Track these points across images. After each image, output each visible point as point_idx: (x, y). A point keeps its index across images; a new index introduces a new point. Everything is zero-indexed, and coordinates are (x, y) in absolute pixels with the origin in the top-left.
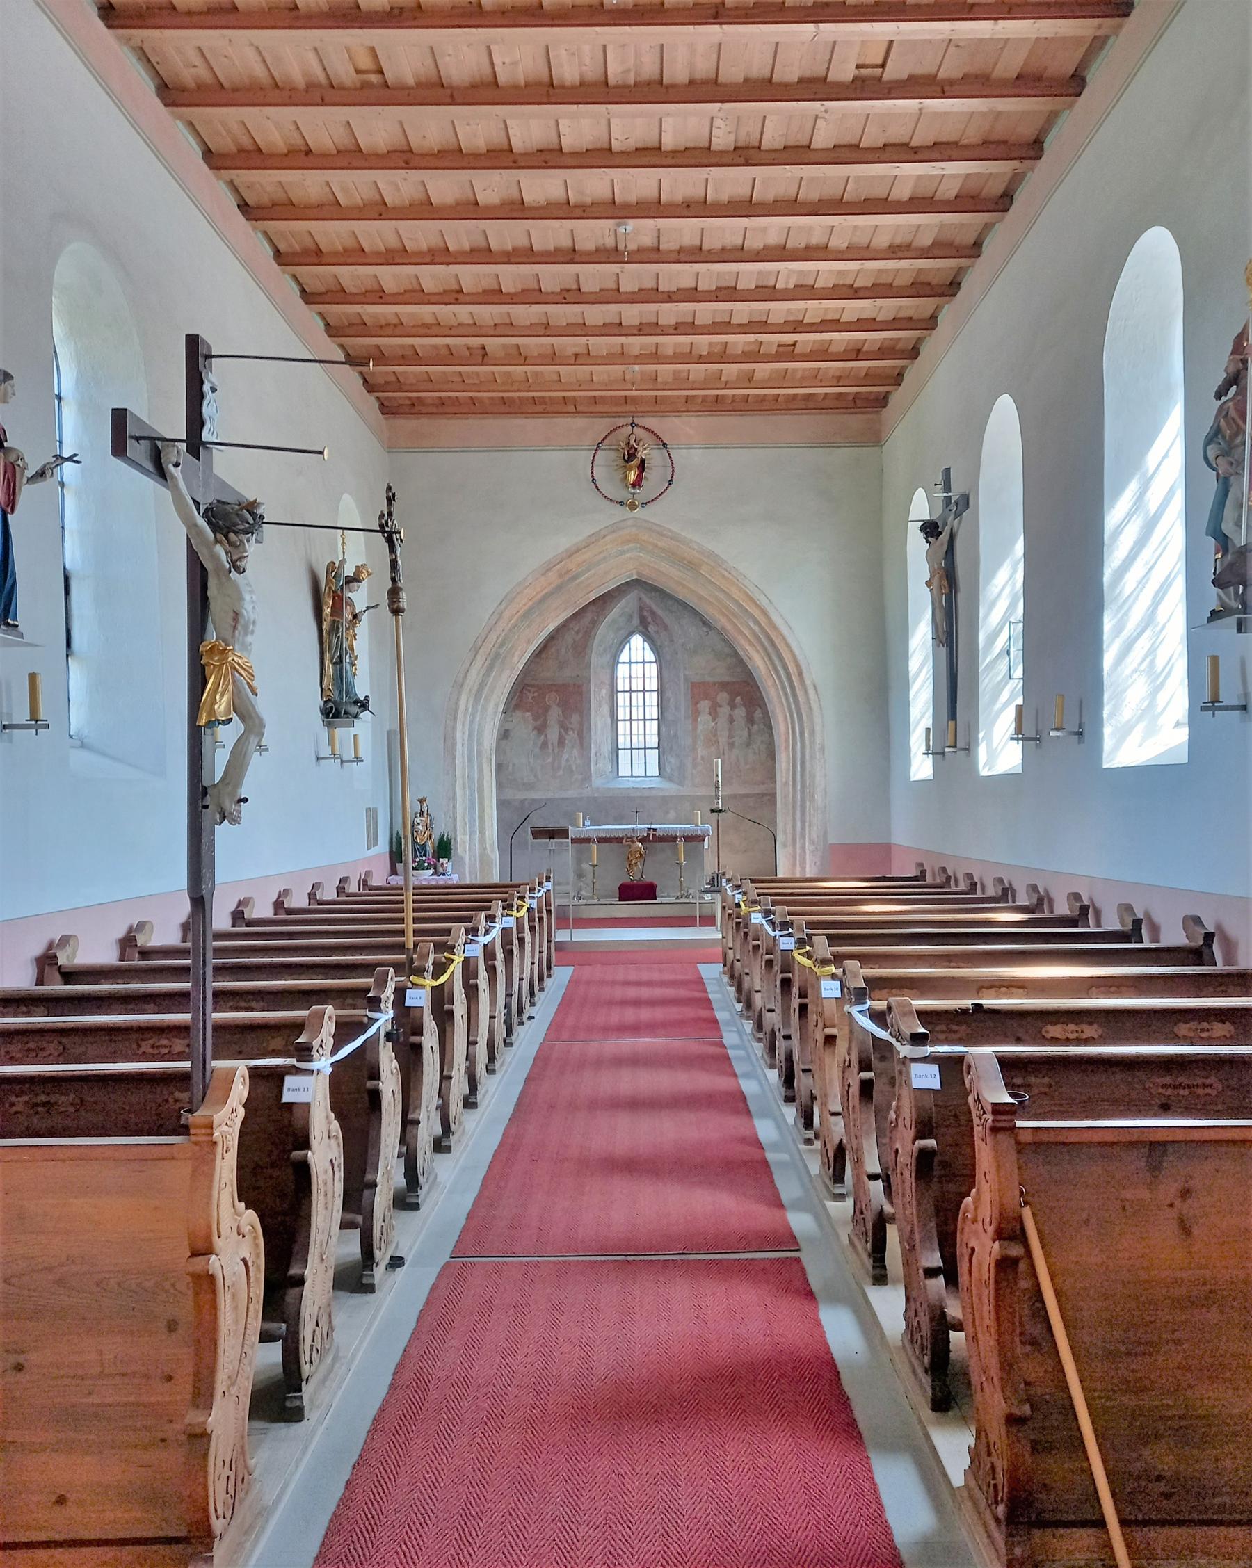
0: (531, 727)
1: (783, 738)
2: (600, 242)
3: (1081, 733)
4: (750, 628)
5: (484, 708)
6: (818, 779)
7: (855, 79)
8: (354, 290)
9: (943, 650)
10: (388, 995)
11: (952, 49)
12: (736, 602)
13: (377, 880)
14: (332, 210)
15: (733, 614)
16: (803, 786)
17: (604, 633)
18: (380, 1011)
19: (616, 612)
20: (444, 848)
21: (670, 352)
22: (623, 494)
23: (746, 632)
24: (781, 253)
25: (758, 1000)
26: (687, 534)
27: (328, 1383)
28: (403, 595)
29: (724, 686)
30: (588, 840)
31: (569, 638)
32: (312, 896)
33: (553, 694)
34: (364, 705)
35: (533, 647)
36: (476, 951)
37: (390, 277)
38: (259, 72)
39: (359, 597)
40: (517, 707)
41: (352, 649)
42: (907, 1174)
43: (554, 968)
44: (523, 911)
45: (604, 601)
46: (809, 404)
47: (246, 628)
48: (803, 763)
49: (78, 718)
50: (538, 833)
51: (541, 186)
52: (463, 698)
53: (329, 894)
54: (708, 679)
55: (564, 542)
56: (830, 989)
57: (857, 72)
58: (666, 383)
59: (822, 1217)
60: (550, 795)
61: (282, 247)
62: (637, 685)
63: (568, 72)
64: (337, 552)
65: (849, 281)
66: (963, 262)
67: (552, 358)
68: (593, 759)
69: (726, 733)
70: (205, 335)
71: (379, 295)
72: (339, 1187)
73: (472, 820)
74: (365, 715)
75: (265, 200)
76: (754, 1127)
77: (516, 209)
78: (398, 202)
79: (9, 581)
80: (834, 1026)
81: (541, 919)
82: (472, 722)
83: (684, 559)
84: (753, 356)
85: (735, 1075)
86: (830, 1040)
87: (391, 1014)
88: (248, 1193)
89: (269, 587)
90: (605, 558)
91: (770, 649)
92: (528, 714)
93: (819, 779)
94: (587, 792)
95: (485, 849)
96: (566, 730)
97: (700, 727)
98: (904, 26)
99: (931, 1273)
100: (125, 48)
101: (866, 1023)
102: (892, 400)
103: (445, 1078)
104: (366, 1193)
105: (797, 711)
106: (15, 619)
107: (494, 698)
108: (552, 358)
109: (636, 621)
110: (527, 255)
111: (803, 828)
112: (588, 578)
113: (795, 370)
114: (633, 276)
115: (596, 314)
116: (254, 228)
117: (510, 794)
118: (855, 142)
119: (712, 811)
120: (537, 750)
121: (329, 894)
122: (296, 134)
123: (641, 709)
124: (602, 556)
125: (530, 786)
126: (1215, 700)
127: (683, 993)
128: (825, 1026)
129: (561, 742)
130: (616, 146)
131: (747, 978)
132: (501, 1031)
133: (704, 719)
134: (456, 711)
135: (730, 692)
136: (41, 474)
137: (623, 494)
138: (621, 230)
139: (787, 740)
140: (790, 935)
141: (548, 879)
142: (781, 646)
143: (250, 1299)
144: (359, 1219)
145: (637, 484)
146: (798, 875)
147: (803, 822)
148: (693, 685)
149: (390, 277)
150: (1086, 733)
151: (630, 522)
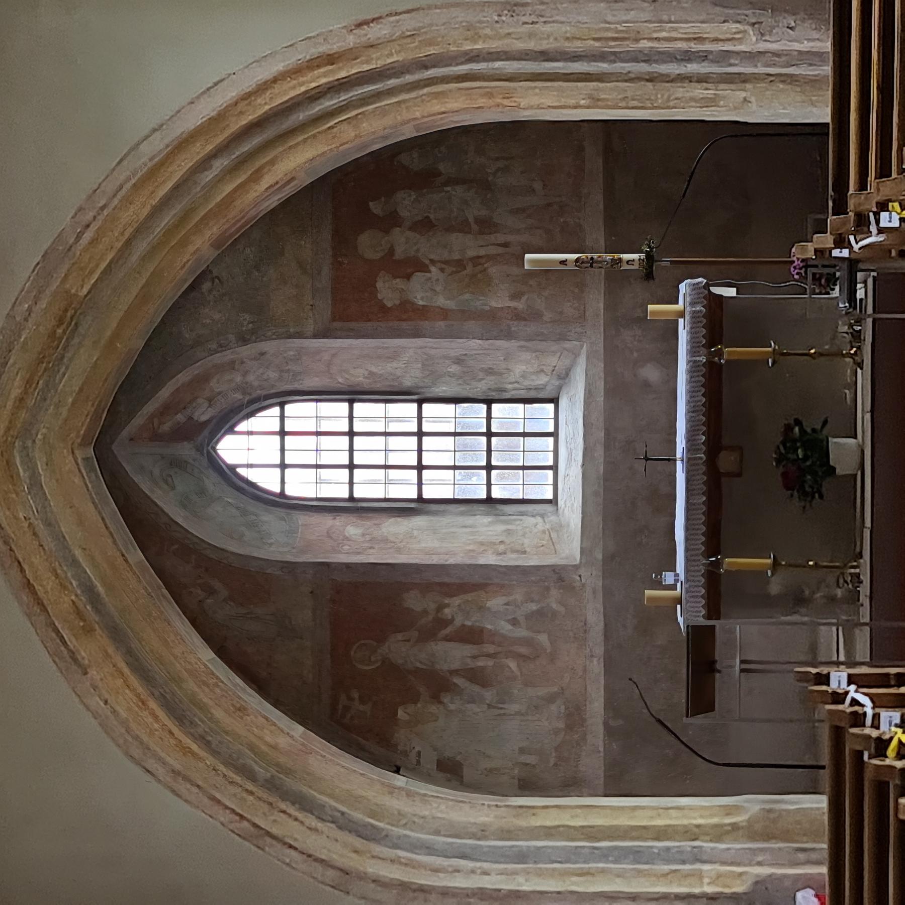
0: (433, 708)
4: (220, 179)
5: (398, 818)
17: (215, 527)
23: (229, 188)
29: (343, 242)
40: (385, 741)
45: (143, 524)
50: (701, 699)
60: (597, 667)
62: (335, 450)
68: (512, 560)
69: (456, 240)
73: (666, 856)
82: (430, 850)
83: (52, 335)
90: (48, 524)
92: (401, 713)
94: (591, 579)
95: (735, 827)
97: (441, 301)
109: (185, 450)
111: (704, 57)
112: (92, 559)
117: (592, 764)
120: (489, 695)
123: (394, 442)
124: (40, 527)
125: (575, 717)
129: (472, 636)
133: (419, 291)
134: (404, 886)
141: (824, 679)
142: (264, 105)
146: (827, 69)
147: (687, 57)
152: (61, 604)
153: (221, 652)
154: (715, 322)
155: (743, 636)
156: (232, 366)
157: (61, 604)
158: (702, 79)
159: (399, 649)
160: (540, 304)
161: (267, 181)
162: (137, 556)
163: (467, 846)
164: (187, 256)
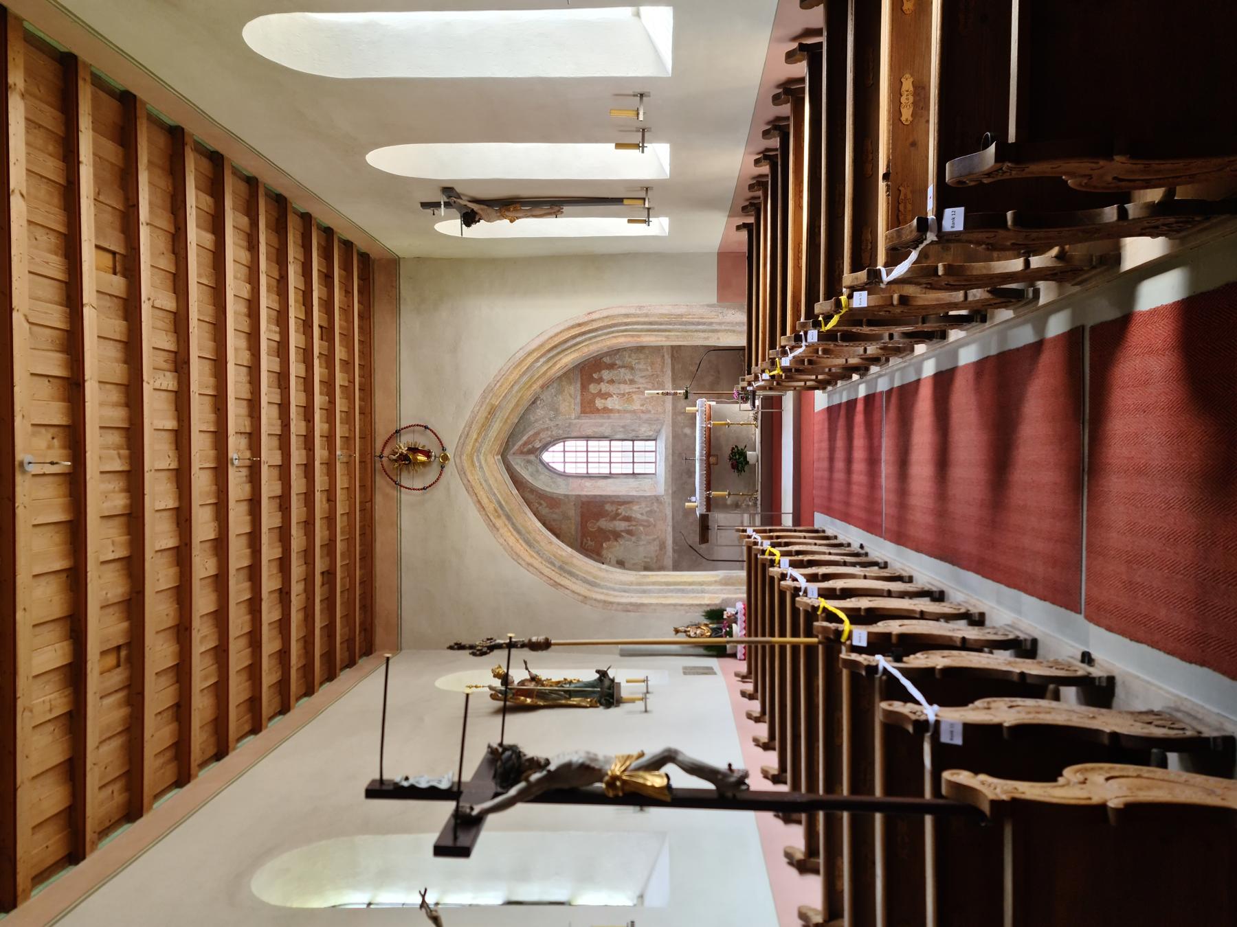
1: (629, 339)
3: (642, 95)
6: (664, 311)
7: (124, 276)
8: (279, 674)
9: (566, 209)
10: (862, 659)
11: (101, 198)
12: (521, 376)
13: (743, 667)
14: (220, 690)
15: (531, 377)
16: (667, 323)
17: (541, 483)
18: (877, 667)
19: (525, 474)
20: (715, 615)
21: (326, 426)
22: (435, 468)
23: (545, 368)
24: (253, 337)
25: (853, 361)
26: (467, 415)
27: (1200, 716)
28: (534, 639)
29: (584, 387)
30: (708, 499)
31: (544, 511)
32: (757, 720)
33: (589, 525)
34: (603, 674)
36: (813, 587)
38: (116, 743)
39: (518, 675)
42: (1034, 235)
43: (816, 527)
44: (776, 551)
48: (651, 323)
51: (203, 526)
53: (755, 706)
55: (473, 514)
56: (861, 300)
60: (670, 529)
61: (247, 728)
63: (119, 502)
64: (482, 693)
65: (274, 283)
66: (261, 192)
67: (330, 519)
68: (641, 494)
69: (622, 386)
70: (364, 784)
71: (283, 655)
72: (1030, 702)
73: (693, 591)
74: (611, 674)
75: (212, 740)
76: (966, 366)
77: (220, 545)
78: (215, 637)
81: (778, 537)
82: (614, 590)
84: (329, 359)
85: (918, 381)
86: (904, 300)
87: (879, 657)
88: (1050, 775)
89: (551, 738)
91: (559, 349)
93: (664, 311)
94: (668, 500)
96: (618, 514)
97: (617, 407)
98: (85, 236)
99: (1123, 214)
100: (100, 845)
101: (901, 270)
102: (364, 250)
103: (923, 616)
105: (611, 327)
107: (594, 571)
108: (330, 519)
109: (532, 457)
110: (254, 539)
111: (704, 324)
113: (341, 327)
114: (270, 455)
115: (297, 484)
116: (234, 749)
118: (171, 277)
119: (686, 398)
120: (634, 539)
121: (755, 706)
122: (165, 715)
125: (662, 546)
127: (842, 422)
129: (627, 519)
130: (174, 465)
131: (833, 370)
132: (874, 571)
133: (611, 403)
134: (605, 602)
137: (435, 468)
138: (236, 462)
139: (632, 336)
140: (806, 333)
143: (1138, 776)
144: (1051, 687)
145: (427, 454)
146: (745, 328)
147: (699, 324)
148: (583, 412)
149: (270, 645)
151: (458, 461)
152: (490, 508)
153: (544, 524)
157: (490, 508)
158: (704, 331)
160: (650, 408)
161: (558, 366)
162: (515, 492)
164: (532, 391)
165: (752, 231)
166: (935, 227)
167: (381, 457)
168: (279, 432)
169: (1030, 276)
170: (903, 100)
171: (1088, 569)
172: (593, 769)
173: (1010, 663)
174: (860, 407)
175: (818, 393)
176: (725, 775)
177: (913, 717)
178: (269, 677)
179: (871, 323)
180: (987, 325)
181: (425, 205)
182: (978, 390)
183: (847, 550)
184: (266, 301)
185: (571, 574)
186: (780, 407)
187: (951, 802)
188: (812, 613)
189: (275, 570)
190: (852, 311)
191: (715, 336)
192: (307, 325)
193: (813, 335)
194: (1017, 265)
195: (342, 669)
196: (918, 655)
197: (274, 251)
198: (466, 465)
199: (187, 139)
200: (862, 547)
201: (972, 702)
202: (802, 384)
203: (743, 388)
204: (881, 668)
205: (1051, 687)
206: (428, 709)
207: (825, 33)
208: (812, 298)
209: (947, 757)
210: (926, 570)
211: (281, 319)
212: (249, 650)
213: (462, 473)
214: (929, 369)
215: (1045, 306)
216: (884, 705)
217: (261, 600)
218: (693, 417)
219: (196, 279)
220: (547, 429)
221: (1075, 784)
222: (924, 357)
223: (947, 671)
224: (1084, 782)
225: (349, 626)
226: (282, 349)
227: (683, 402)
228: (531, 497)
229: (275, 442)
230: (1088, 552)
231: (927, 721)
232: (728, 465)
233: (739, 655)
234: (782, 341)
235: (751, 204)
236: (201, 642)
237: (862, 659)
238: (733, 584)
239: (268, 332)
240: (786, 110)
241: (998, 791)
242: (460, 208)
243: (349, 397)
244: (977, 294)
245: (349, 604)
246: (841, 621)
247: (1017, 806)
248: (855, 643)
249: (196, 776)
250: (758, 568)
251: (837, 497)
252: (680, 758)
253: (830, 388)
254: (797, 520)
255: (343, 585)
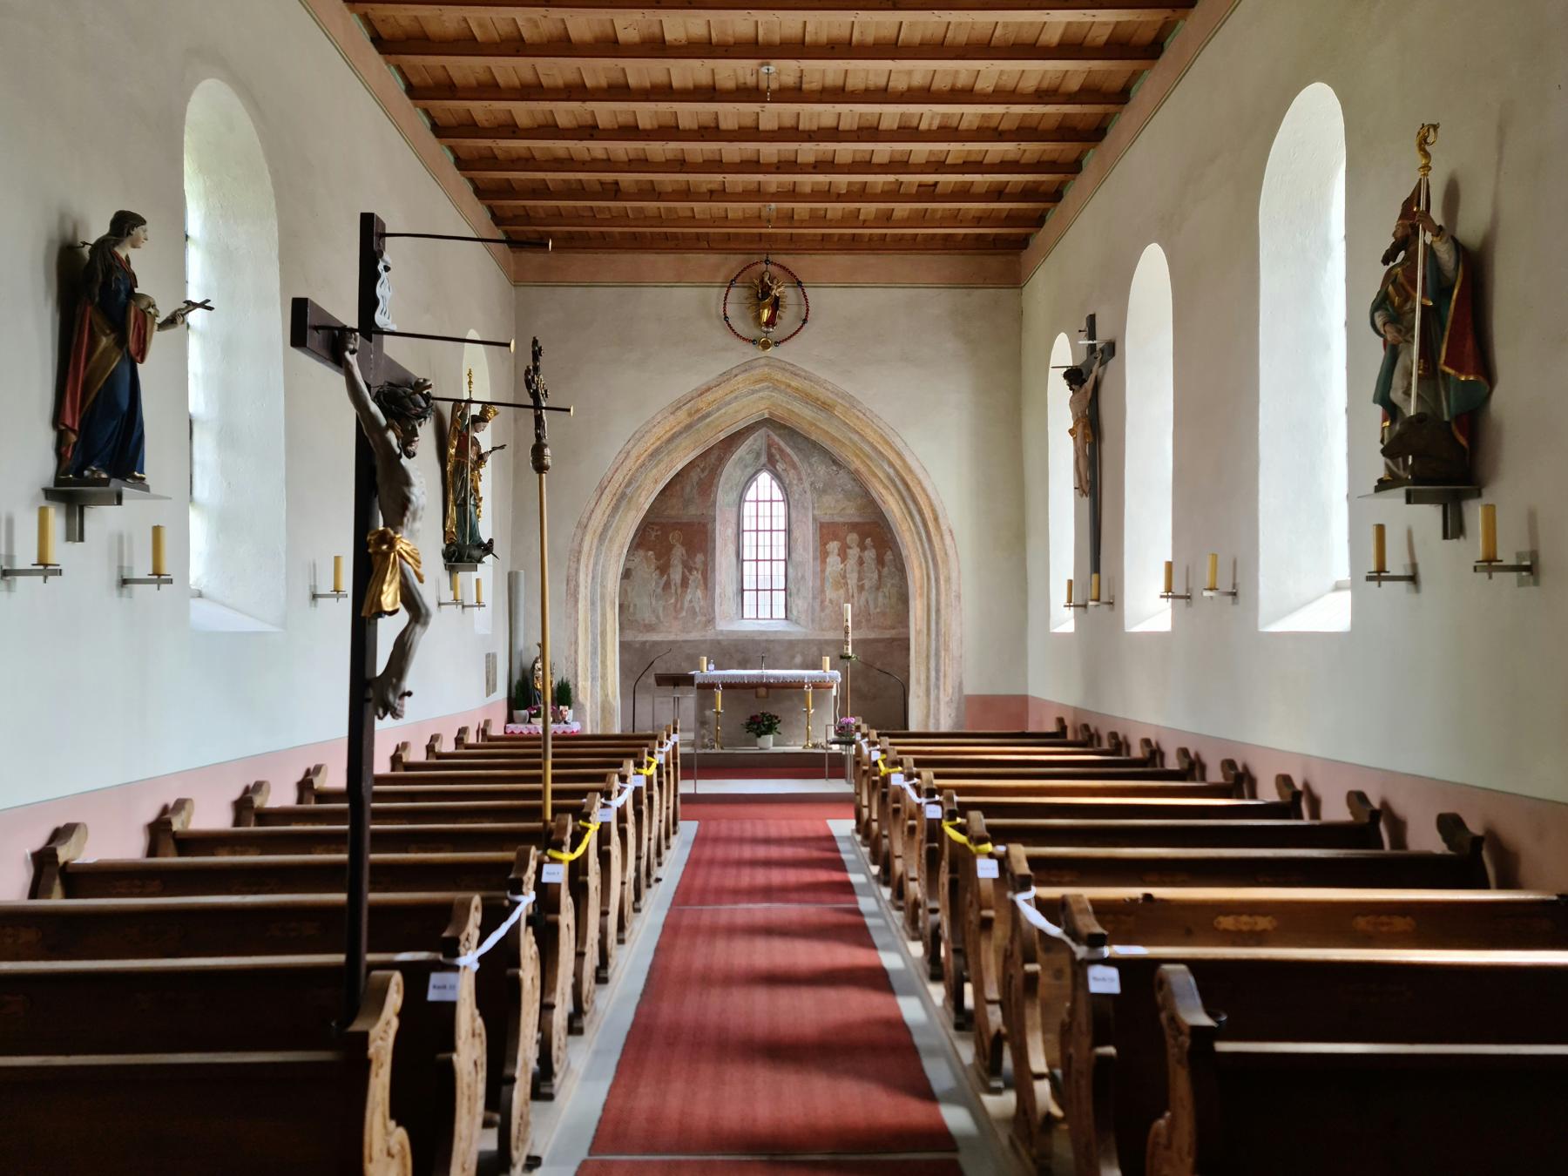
2: (741, 80)
3: (1234, 594)
4: (885, 471)
8: (486, 124)
9: (1086, 501)
10: (530, 875)
13: (497, 730)
17: (731, 471)
18: (520, 892)
19: (742, 451)
20: (564, 695)
21: (808, 189)
22: (754, 332)
23: (881, 475)
25: (898, 866)
26: (822, 374)
28: (547, 451)
29: (854, 527)
31: (695, 476)
32: (430, 748)
34: (488, 548)
35: (661, 486)
36: (611, 816)
37: (524, 112)
39: (485, 438)
41: (477, 491)
42: (1083, 1082)
43: (680, 823)
44: (653, 770)
46: (947, 245)
47: (414, 514)
48: (938, 611)
49: (198, 571)
52: (588, 539)
53: (447, 746)
54: (838, 519)
55: (694, 381)
56: (987, 869)
57: (1387, 268)
58: (802, 221)
59: (978, 1112)
60: (671, 637)
61: (415, 80)
65: (993, 124)
66: (1110, 108)
67: (687, 194)
69: (855, 575)
71: (510, 129)
72: (481, 1088)
73: (594, 666)
74: (488, 559)
76: (897, 1007)
79: (136, 434)
80: (990, 908)
81: (668, 773)
82: (596, 564)
84: (894, 194)
85: (873, 947)
86: (987, 924)
88: (398, 1112)
91: (905, 493)
94: (710, 634)
96: (690, 570)
97: (829, 569)
102: (1032, 242)
103: (580, 955)
104: (505, 1089)
105: (933, 560)
106: (141, 472)
108: (687, 194)
109: (764, 459)
110: (663, 92)
111: (937, 679)
113: (934, 211)
114: (772, 114)
115: (732, 151)
116: (387, 62)
119: (842, 657)
120: (659, 590)
121: (447, 746)
123: (768, 549)
125: (650, 628)
126: (1381, 568)
128: (981, 908)
129: (685, 583)
131: (885, 841)
133: (833, 561)
134: (580, 552)
135: (868, 536)
136: (171, 321)
137: (754, 332)
138: (764, 70)
140: (937, 803)
144: (497, 1117)
145: (771, 322)
146: (932, 730)
147: (937, 671)
148: (822, 525)
149: (524, 112)
150: (1241, 592)
151: (763, 361)
152: (701, 403)
154: (820, 687)
155: (689, 699)
156: (800, 479)
157: (701, 403)
158: (928, 678)
159: (679, 552)
161: (884, 492)
162: (722, 436)
163: (597, 579)
165: (1058, 737)
166: (1094, 956)
167: (767, 262)
168: (801, 127)
169: (1022, 1081)
170: (1245, 918)
171: (648, 1162)
172: (404, 515)
173: (526, 1064)
174: (837, 876)
175: (852, 823)
176: (396, 687)
177: (463, 938)
178: (481, 110)
179: (953, 884)
180: (952, 1031)
181: (1092, 320)
182: (869, 1023)
183: (654, 861)
184: (971, 113)
185: (616, 509)
186: (832, 776)
187: (363, 983)
188: (582, 814)
189: (622, 119)
190: (972, 858)
191: (922, 693)
192: (939, 166)
193: (933, 812)
194: (1038, 1063)
195: (490, 208)
196: (535, 947)
197: (1034, 124)
198: (757, 373)
199: (1180, 12)
200: (658, 880)
201: (481, 1014)
202: (865, 802)
203: (858, 728)
204: (519, 898)
205: (497, 1117)
206: (451, 314)
207: (1316, 822)
208: (989, 810)
209: (416, 978)
210: (632, 962)
211: (947, 132)
212: (517, 83)
213: (747, 367)
214: (890, 961)
215: (980, 1102)
216: (476, 900)
217: (584, 101)
218: (817, 665)
219: (1001, 20)
220: (800, 479)
221: (387, 1142)
222: (905, 955)
223: (516, 984)
224: (390, 1154)
225: (544, 220)
226: (908, 132)
227: (836, 653)
228: (713, 458)
229: (788, 122)
230: (669, 1163)
231: (458, 955)
232: (757, 711)
233: (511, 727)
234: (927, 773)
235: (1091, 736)
236: (529, 20)
237: (530, 875)
238: (604, 718)
239: (930, 114)
240: (1215, 776)
241: (379, 1042)
242: (1088, 365)
243: (845, 221)
244: (995, 1017)
245: (576, 217)
246: (573, 850)
247: (362, 1067)
248: (546, 868)
249: (352, 10)
250: (632, 746)
251: (720, 852)
252: (418, 629)
253: (859, 838)
254: (688, 799)
255: (601, 210)
